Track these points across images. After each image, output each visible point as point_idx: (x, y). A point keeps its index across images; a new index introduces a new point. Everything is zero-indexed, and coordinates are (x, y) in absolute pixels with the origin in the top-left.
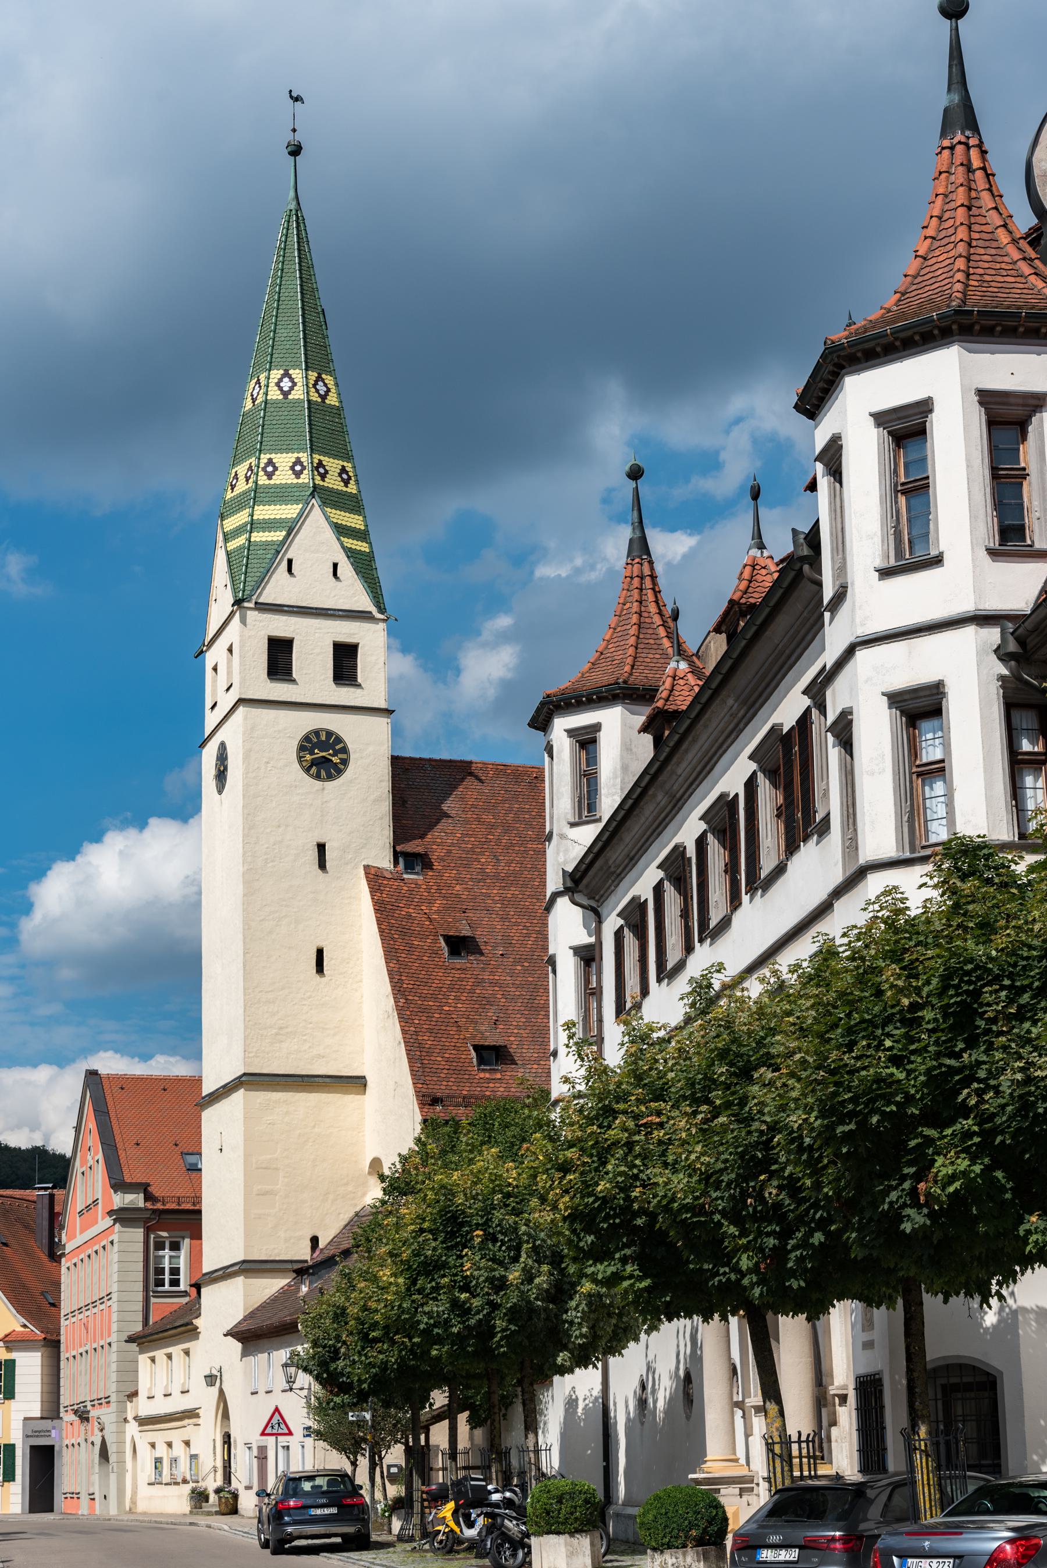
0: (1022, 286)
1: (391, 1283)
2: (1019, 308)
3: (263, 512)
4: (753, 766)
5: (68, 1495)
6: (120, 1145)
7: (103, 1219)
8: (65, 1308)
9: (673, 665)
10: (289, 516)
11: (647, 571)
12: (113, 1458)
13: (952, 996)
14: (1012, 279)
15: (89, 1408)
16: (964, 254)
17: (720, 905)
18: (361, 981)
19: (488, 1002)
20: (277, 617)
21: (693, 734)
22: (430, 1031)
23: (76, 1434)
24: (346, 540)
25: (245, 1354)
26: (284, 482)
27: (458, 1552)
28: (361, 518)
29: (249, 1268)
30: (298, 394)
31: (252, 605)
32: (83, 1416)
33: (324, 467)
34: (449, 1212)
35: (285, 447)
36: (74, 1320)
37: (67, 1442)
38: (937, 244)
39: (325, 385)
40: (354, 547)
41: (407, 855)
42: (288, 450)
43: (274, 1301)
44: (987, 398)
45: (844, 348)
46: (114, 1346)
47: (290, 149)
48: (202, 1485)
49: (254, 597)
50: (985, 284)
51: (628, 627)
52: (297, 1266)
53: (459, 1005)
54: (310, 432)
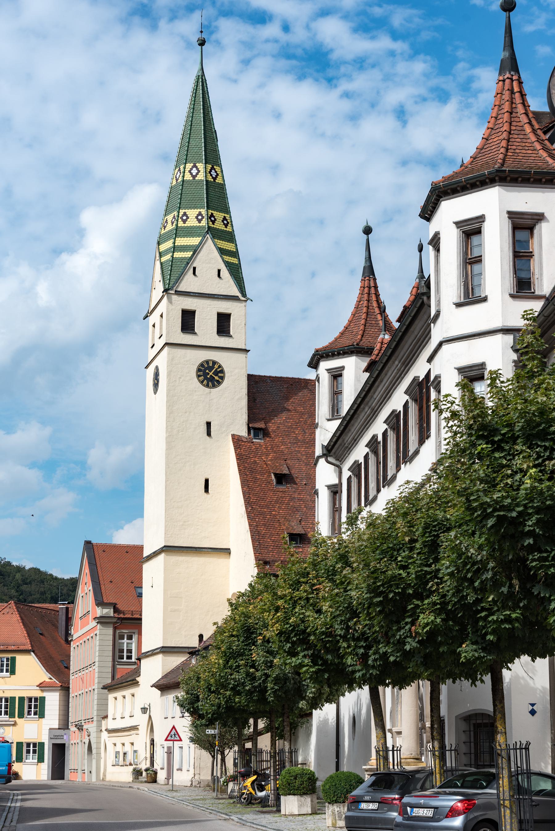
0: (535, 155)
1: (216, 663)
2: (532, 168)
3: (181, 241)
4: (407, 397)
5: (72, 771)
6: (102, 582)
7: (92, 622)
8: (72, 669)
9: (381, 336)
10: (194, 244)
11: (372, 284)
12: (94, 751)
13: (427, 537)
14: (531, 152)
15: (83, 724)
16: (506, 138)
17: (393, 467)
18: (229, 497)
19: (296, 510)
20: (187, 299)
21: (380, 378)
22: (264, 525)
23: (76, 738)
24: (225, 257)
25: (162, 695)
26: (192, 225)
27: (253, 804)
28: (234, 245)
29: (166, 650)
30: (201, 176)
31: (173, 292)
32: (80, 728)
33: (214, 217)
34: (245, 627)
35: (193, 206)
36: (77, 676)
37: (72, 742)
38: (494, 132)
39: (216, 172)
40: (229, 261)
41: (255, 429)
42: (195, 208)
43: (177, 669)
44: (512, 215)
45: (441, 188)
46: (96, 691)
47: (199, 42)
48: (140, 767)
49: (175, 288)
50: (516, 155)
51: (361, 314)
52: (190, 650)
53: (281, 511)
54: (207, 198)
